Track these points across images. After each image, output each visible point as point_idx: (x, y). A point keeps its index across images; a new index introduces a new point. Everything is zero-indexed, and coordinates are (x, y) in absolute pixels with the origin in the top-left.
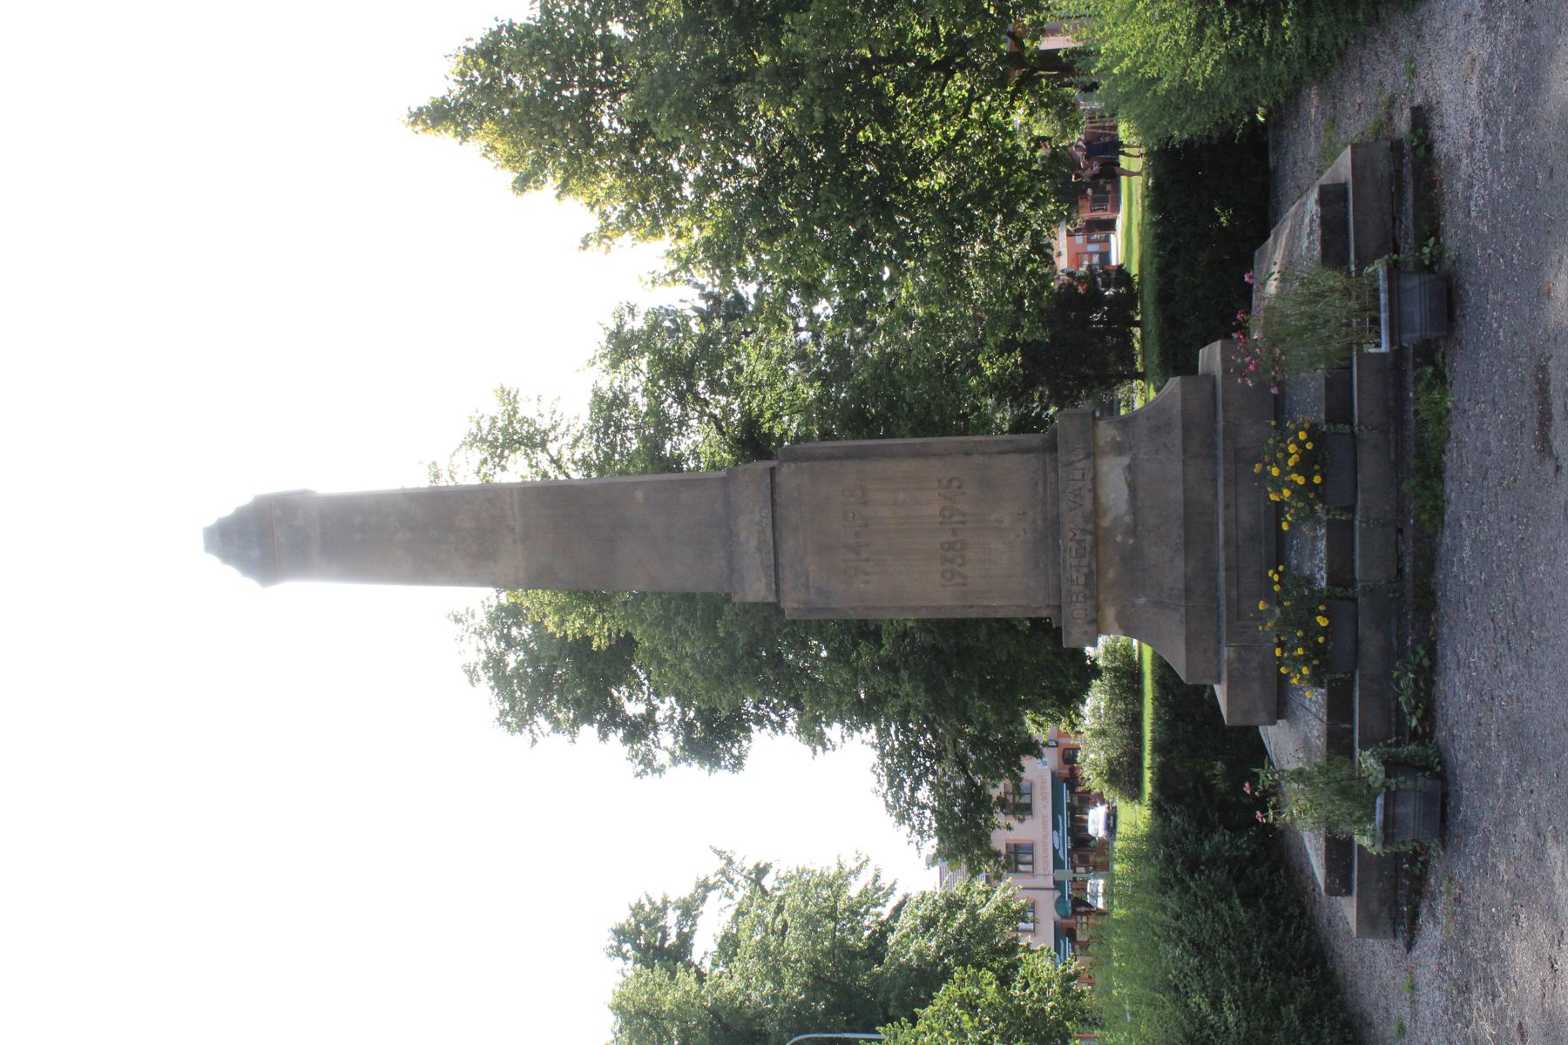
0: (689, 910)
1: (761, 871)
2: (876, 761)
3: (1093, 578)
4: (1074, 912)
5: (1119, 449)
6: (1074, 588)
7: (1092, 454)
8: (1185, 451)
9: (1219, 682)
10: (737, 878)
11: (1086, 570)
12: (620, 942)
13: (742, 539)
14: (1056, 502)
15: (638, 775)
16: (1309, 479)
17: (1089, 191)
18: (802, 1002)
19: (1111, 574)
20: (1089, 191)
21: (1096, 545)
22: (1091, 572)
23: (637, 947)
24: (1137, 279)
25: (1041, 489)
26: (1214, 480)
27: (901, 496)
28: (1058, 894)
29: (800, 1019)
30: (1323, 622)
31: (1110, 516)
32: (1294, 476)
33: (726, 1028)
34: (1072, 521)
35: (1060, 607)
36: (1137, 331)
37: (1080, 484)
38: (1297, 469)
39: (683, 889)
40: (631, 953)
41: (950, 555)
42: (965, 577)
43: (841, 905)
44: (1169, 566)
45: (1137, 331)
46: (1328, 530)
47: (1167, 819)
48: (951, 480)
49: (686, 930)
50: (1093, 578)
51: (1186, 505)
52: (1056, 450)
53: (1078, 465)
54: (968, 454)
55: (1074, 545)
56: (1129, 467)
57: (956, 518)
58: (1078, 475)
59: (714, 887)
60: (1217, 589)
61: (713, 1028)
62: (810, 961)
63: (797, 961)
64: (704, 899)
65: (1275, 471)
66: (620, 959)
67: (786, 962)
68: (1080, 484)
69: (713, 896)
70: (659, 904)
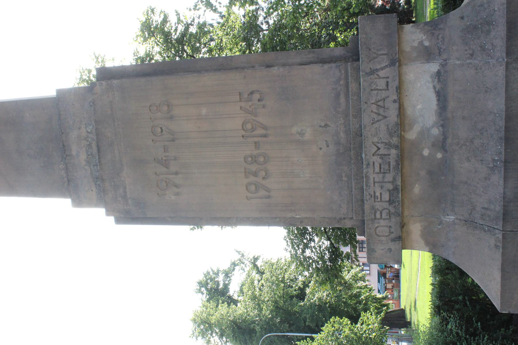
0: (227, 274)
1: (256, 259)
2: (286, 234)
3: (397, 194)
5: (428, 54)
6: (378, 205)
7: (397, 62)
10: (246, 262)
11: (391, 187)
12: (200, 287)
13: (74, 153)
14: (358, 114)
15: (191, 229)
18: (270, 318)
19: (417, 189)
21: (401, 159)
22: (396, 189)
23: (207, 289)
25: (342, 100)
27: (204, 111)
29: (269, 326)
31: (417, 128)
33: (239, 328)
34: (376, 134)
35: (363, 222)
37: (384, 94)
39: (225, 266)
40: (205, 292)
41: (253, 168)
42: (268, 190)
43: (286, 276)
47: (444, 321)
48: (252, 93)
49: (227, 282)
50: (397, 194)
51: (508, 118)
52: (358, 60)
53: (382, 73)
54: (268, 66)
55: (377, 160)
56: (439, 73)
58: (382, 84)
59: (238, 265)
61: (234, 328)
62: (272, 302)
63: (268, 301)
64: (234, 269)
66: (200, 294)
67: (264, 301)
68: (384, 94)
69: (237, 268)
70: (216, 271)
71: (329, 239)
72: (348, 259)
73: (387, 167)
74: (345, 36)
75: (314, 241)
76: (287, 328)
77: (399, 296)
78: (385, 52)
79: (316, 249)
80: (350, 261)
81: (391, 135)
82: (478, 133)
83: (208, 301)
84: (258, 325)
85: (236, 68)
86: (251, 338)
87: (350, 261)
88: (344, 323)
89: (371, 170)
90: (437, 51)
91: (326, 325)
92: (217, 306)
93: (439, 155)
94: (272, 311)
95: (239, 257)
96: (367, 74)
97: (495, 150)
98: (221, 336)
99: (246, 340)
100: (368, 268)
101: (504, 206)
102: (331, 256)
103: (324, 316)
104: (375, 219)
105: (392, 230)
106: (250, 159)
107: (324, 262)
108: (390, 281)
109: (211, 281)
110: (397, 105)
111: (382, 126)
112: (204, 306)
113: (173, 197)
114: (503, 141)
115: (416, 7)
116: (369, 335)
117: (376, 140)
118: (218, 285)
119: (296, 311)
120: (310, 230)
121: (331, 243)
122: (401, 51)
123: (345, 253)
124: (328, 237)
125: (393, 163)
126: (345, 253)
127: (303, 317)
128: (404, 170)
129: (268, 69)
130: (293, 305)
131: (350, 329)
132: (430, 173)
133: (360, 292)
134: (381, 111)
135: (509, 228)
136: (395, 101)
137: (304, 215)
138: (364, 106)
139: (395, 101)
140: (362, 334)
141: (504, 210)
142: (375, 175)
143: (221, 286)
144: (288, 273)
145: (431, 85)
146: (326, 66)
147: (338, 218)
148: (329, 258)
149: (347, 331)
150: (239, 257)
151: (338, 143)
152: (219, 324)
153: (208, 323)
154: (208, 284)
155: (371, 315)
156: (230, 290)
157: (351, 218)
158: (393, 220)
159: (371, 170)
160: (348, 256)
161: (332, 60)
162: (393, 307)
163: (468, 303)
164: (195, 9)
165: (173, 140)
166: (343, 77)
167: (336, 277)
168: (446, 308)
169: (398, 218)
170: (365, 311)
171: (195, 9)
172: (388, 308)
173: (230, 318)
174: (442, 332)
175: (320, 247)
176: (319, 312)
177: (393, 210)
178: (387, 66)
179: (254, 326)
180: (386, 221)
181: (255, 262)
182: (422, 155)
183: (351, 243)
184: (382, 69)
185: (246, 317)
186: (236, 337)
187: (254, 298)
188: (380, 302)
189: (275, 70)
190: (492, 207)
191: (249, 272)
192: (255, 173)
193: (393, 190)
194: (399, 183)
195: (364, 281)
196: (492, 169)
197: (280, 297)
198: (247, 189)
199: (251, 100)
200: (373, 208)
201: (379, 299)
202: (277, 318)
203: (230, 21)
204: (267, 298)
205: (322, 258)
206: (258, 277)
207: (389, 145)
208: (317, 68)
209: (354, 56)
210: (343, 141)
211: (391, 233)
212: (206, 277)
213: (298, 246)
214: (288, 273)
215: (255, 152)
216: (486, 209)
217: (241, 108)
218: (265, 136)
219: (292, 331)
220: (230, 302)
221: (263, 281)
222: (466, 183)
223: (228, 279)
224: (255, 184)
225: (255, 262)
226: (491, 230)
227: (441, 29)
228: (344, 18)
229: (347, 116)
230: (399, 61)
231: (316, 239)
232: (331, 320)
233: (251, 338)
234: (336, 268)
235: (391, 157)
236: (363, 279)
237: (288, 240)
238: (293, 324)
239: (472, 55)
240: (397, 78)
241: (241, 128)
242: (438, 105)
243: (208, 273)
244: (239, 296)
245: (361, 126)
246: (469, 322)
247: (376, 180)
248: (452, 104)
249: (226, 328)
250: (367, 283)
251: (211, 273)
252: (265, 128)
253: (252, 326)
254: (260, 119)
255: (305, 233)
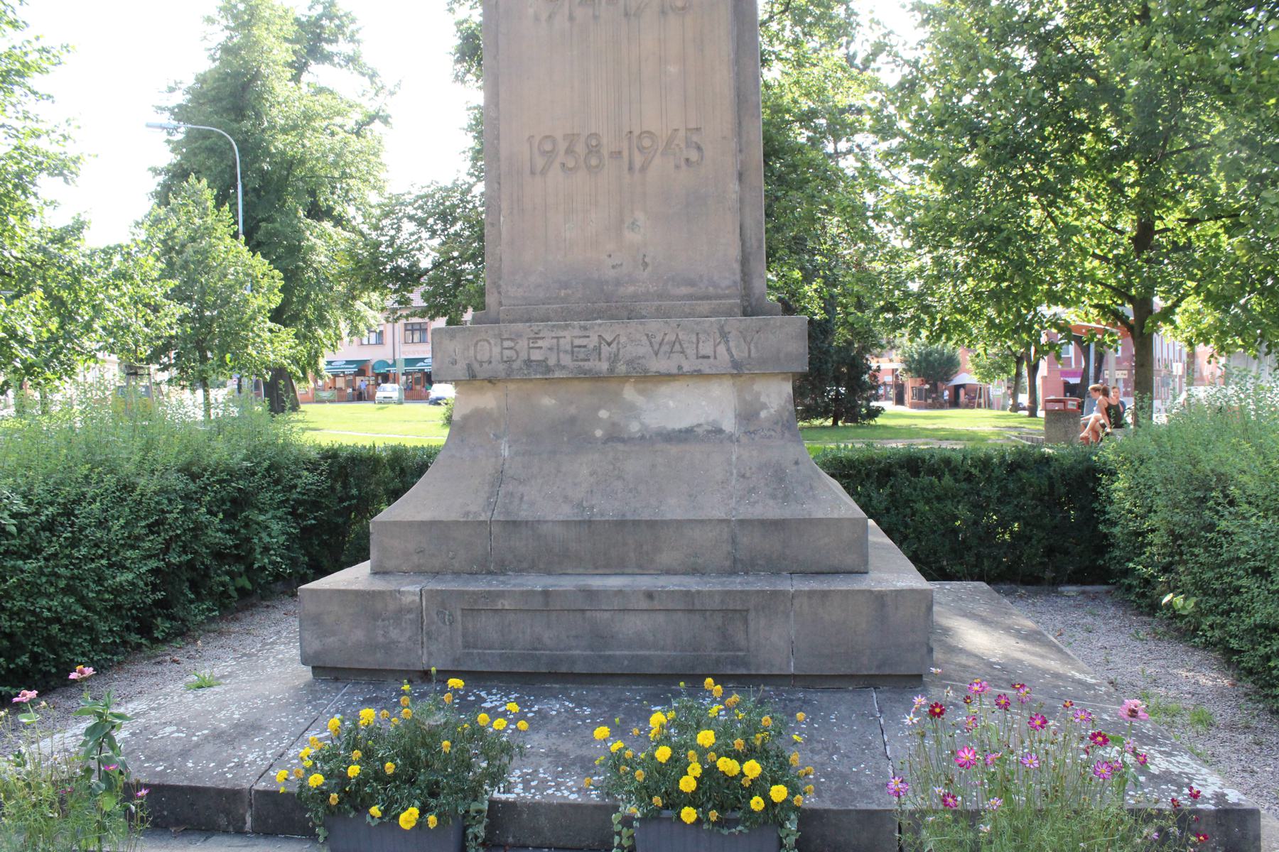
0: (351, 60)
1: (385, 120)
3: (541, 373)
4: (378, 375)
5: (747, 416)
6: (523, 344)
7: (738, 371)
8: (742, 522)
9: (375, 573)
11: (552, 362)
16: (692, 800)
17: (927, 386)
19: (548, 401)
20: (927, 386)
21: (596, 377)
22: (549, 370)
23: (320, 18)
24: (872, 423)
25: (684, 290)
26: (694, 571)
27: (673, 69)
28: (391, 362)
29: (252, 148)
30: (409, 818)
31: (639, 400)
32: (695, 769)
33: (245, 87)
34: (632, 341)
35: (497, 321)
36: (829, 422)
37: (691, 352)
38: (710, 772)
39: (368, 58)
42: (544, 172)
44: (552, 498)
45: (829, 422)
46: (596, 807)
47: (313, 466)
48: (699, 148)
49: (336, 59)
50: (541, 373)
51: (652, 524)
52: (745, 314)
53: (722, 349)
54: (741, 176)
55: (593, 342)
56: (720, 431)
57: (638, 160)
58: (706, 349)
59: (373, 82)
60: (520, 571)
61: (244, 75)
63: (304, 146)
65: (706, 738)
67: (302, 136)
68: (691, 352)
71: (436, 265)
72: (400, 303)
73: (582, 356)
74: (811, 298)
75: (432, 237)
76: (251, 185)
77: (322, 401)
78: (753, 354)
79: (416, 241)
80: (396, 305)
81: (629, 363)
82: (631, 486)
83: (297, 20)
84: (253, 125)
85: (740, 123)
86: (226, 110)
87: (396, 305)
88: (272, 297)
89: (577, 332)
90: (752, 429)
91: (267, 262)
92: (286, 40)
93: (599, 433)
94: (283, 153)
95: (390, 87)
96: (722, 327)
97: (607, 508)
98: (226, 50)
99: (221, 100)
100: (373, 340)
101: (527, 522)
102: (404, 270)
103: (279, 258)
104: (502, 340)
105: (485, 365)
106: (594, 143)
107: (391, 257)
108: (350, 384)
109: (337, 26)
110: (675, 371)
111: (644, 350)
112: (286, 12)
113: (531, 11)
114: (619, 518)
115: (862, 426)
116: (253, 344)
117: (623, 339)
118: (329, 41)
119: (285, 201)
120: (452, 231)
121: (427, 271)
122: (754, 377)
123: (411, 296)
124: (440, 264)
125: (587, 365)
126: (411, 296)
127: (276, 215)
128: (576, 382)
129: (736, 176)
130: (298, 194)
131: (261, 308)
132: (573, 420)
133: (330, 327)
134: (665, 348)
135: (495, 529)
136: (680, 368)
137: (504, 230)
138: (673, 322)
139: (680, 368)
140: (252, 331)
141: (521, 522)
142: (569, 339)
143: (327, 48)
144: (360, 186)
145: (702, 421)
146: (737, 267)
147: (501, 283)
148: (399, 267)
149: (258, 301)
150: (390, 87)
151: (618, 283)
152: (251, 44)
153: (250, 21)
154: (331, 19)
155: (291, 348)
156: (321, 66)
157: (500, 304)
158: (502, 367)
159: (577, 332)
160: (405, 302)
161: (746, 275)
162: (300, 388)
163: (345, 504)
164: (872, 20)
165: (626, 14)
166: (720, 291)
167: (365, 281)
168: (336, 469)
169: (503, 375)
170: (297, 336)
171: (872, 20)
172: (299, 380)
173: (263, 66)
174: (296, 462)
175: (420, 249)
176: (285, 247)
177: (515, 366)
178: (732, 356)
179: (250, 117)
180: (499, 357)
181: (380, 118)
182: (599, 408)
183: (429, 308)
184: (728, 350)
185: (267, 100)
186: (224, 80)
187: (308, 117)
188: (309, 364)
189: (734, 186)
190: (525, 506)
191: (360, 106)
192: (572, 151)
193: (547, 366)
194: (557, 375)
195: (351, 333)
196: (580, 505)
197: (311, 169)
198: (547, 137)
199: (688, 146)
200: (519, 336)
201: (316, 363)
202: (270, 163)
203: (850, 83)
204: (308, 144)
205: (399, 252)
206: (350, 124)
207: (614, 359)
208: (735, 252)
209: (751, 309)
210: (621, 290)
211: (481, 363)
212: (346, 15)
213: (421, 207)
214: (360, 186)
215: (605, 152)
216: (522, 498)
217: (676, 130)
218: (631, 168)
219: (245, 193)
220: (296, 68)
221: (342, 135)
222: (559, 471)
223: (342, 63)
224: (552, 151)
225: (380, 118)
226: (491, 506)
227: (783, 434)
228: (844, 296)
229: (660, 296)
230: (739, 375)
231: (436, 242)
232: (276, 272)
233: (226, 110)
234: (381, 280)
235: (597, 362)
236: (354, 331)
237: (433, 187)
238: (259, 196)
239: (743, 476)
240: (714, 371)
241: (645, 129)
242: (673, 430)
243: (353, 21)
244: (308, 84)
245: (644, 317)
246: (315, 505)
247: (562, 341)
248: (674, 450)
249: (243, 58)
250: (346, 339)
251: (352, 27)
252: (643, 169)
253: (251, 113)
254: (657, 161)
255: (445, 221)
